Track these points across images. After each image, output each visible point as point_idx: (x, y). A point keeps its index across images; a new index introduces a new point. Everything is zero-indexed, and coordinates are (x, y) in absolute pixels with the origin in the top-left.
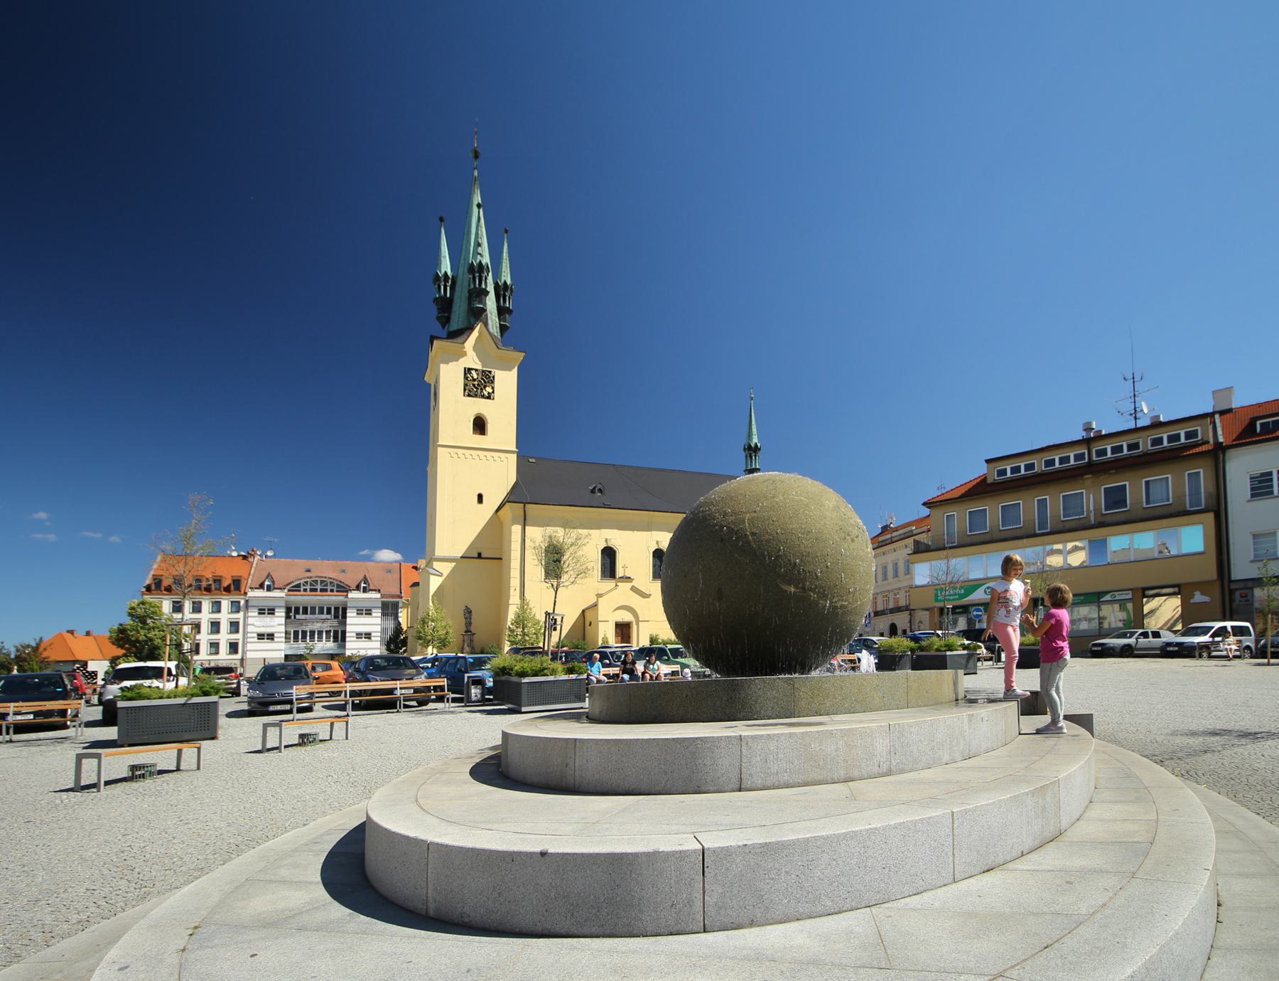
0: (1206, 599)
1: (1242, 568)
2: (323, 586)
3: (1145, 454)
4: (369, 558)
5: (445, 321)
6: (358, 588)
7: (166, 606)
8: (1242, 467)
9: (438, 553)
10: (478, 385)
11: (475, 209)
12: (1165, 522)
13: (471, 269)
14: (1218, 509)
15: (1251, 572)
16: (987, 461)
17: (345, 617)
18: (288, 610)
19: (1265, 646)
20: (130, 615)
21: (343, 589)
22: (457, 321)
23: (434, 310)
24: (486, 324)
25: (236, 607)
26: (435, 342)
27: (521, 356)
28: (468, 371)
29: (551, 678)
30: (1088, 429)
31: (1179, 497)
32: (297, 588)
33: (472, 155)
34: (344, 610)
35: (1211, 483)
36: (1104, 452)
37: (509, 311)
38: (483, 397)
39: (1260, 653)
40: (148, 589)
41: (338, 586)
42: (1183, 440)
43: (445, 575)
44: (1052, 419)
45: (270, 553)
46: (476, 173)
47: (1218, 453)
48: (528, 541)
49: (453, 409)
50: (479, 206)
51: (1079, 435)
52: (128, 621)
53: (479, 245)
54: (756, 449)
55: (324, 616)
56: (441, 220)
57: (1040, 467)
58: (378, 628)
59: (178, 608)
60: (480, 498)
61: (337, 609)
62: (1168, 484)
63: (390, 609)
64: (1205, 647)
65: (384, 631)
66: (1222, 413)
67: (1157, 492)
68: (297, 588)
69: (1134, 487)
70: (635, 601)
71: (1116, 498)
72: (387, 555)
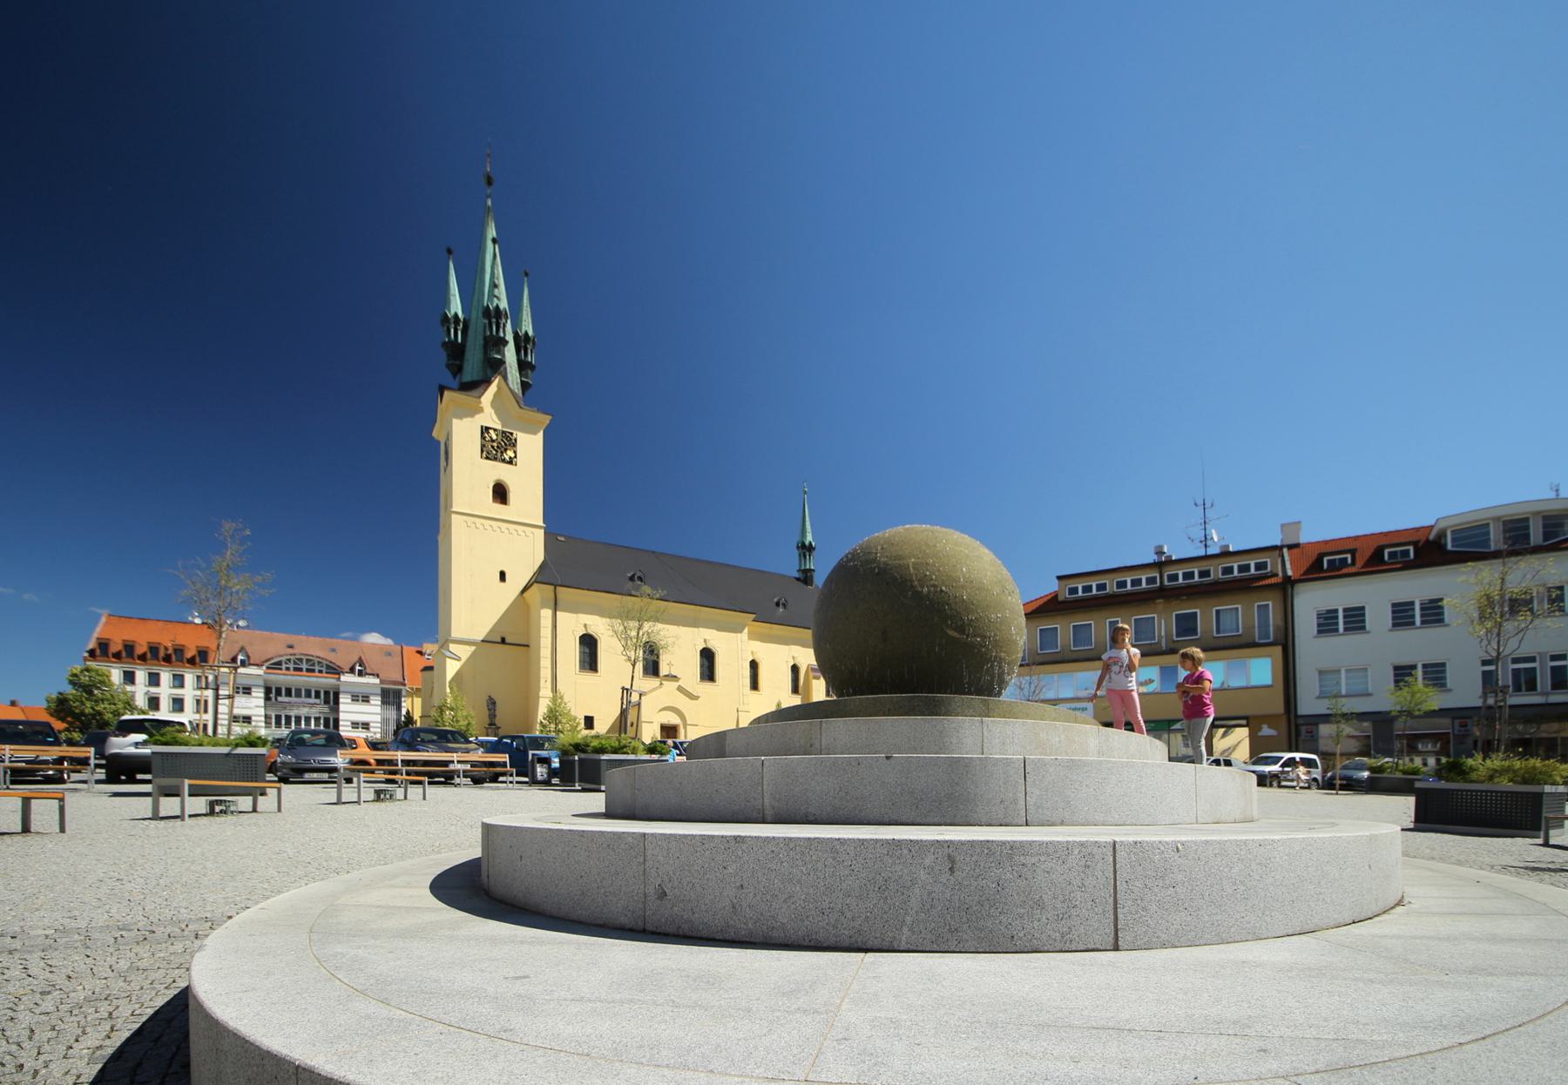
0: (1272, 732)
1: (1308, 704)
2: (312, 666)
3: (1216, 583)
4: (355, 639)
5: (457, 370)
6: (352, 670)
7: (116, 675)
8: (1311, 601)
9: (455, 634)
10: (498, 447)
11: (490, 244)
12: (1235, 652)
13: (487, 312)
14: (1285, 642)
15: (1321, 708)
16: (1059, 578)
17: (337, 702)
18: (268, 691)
19: (1333, 778)
20: (71, 682)
21: (335, 670)
22: (471, 371)
23: (442, 357)
24: (505, 378)
25: (201, 684)
26: (446, 393)
27: (547, 419)
28: (485, 430)
29: (632, 757)
30: (1160, 552)
31: (1249, 628)
32: (277, 665)
33: (484, 181)
34: (337, 695)
35: (1280, 616)
36: (1175, 577)
37: (532, 367)
38: (503, 461)
39: (1328, 785)
40: (92, 653)
41: (328, 667)
42: (1253, 570)
43: (464, 659)
44: (1123, 542)
45: (241, 623)
46: (489, 202)
47: (1286, 587)
48: (561, 629)
49: (468, 474)
50: (494, 241)
51: (1151, 558)
52: (70, 690)
53: (496, 286)
54: (810, 548)
55: (313, 700)
56: (449, 251)
57: (1111, 587)
58: (378, 718)
59: (129, 677)
60: (503, 576)
61: (327, 693)
62: (1239, 614)
63: (391, 697)
64: (1275, 776)
65: (385, 721)
66: (1290, 547)
67: (1227, 620)
68: (277, 665)
69: (1205, 614)
70: (682, 702)
71: (1187, 626)
72: (373, 638)
